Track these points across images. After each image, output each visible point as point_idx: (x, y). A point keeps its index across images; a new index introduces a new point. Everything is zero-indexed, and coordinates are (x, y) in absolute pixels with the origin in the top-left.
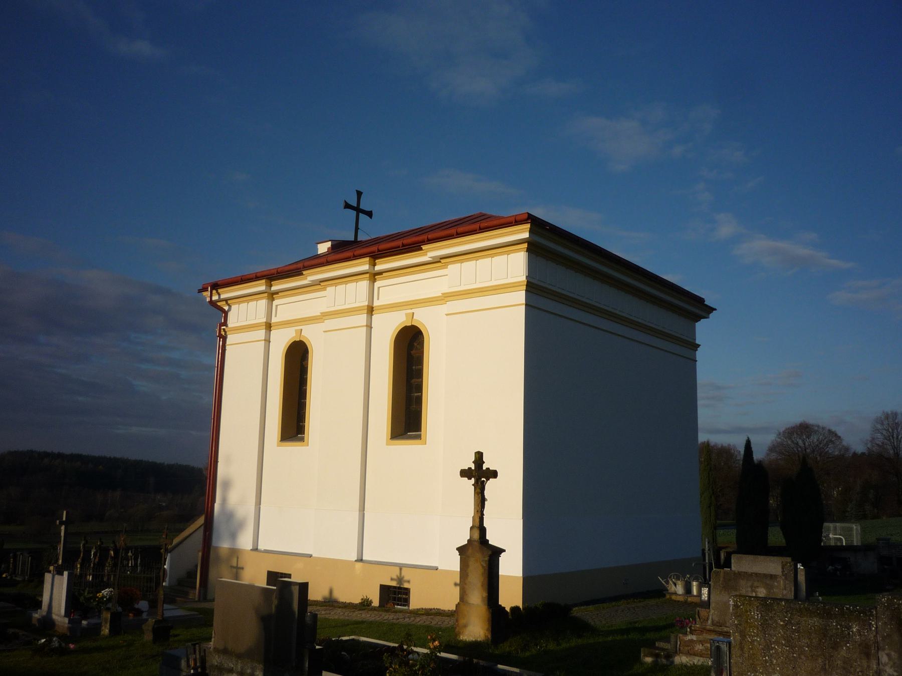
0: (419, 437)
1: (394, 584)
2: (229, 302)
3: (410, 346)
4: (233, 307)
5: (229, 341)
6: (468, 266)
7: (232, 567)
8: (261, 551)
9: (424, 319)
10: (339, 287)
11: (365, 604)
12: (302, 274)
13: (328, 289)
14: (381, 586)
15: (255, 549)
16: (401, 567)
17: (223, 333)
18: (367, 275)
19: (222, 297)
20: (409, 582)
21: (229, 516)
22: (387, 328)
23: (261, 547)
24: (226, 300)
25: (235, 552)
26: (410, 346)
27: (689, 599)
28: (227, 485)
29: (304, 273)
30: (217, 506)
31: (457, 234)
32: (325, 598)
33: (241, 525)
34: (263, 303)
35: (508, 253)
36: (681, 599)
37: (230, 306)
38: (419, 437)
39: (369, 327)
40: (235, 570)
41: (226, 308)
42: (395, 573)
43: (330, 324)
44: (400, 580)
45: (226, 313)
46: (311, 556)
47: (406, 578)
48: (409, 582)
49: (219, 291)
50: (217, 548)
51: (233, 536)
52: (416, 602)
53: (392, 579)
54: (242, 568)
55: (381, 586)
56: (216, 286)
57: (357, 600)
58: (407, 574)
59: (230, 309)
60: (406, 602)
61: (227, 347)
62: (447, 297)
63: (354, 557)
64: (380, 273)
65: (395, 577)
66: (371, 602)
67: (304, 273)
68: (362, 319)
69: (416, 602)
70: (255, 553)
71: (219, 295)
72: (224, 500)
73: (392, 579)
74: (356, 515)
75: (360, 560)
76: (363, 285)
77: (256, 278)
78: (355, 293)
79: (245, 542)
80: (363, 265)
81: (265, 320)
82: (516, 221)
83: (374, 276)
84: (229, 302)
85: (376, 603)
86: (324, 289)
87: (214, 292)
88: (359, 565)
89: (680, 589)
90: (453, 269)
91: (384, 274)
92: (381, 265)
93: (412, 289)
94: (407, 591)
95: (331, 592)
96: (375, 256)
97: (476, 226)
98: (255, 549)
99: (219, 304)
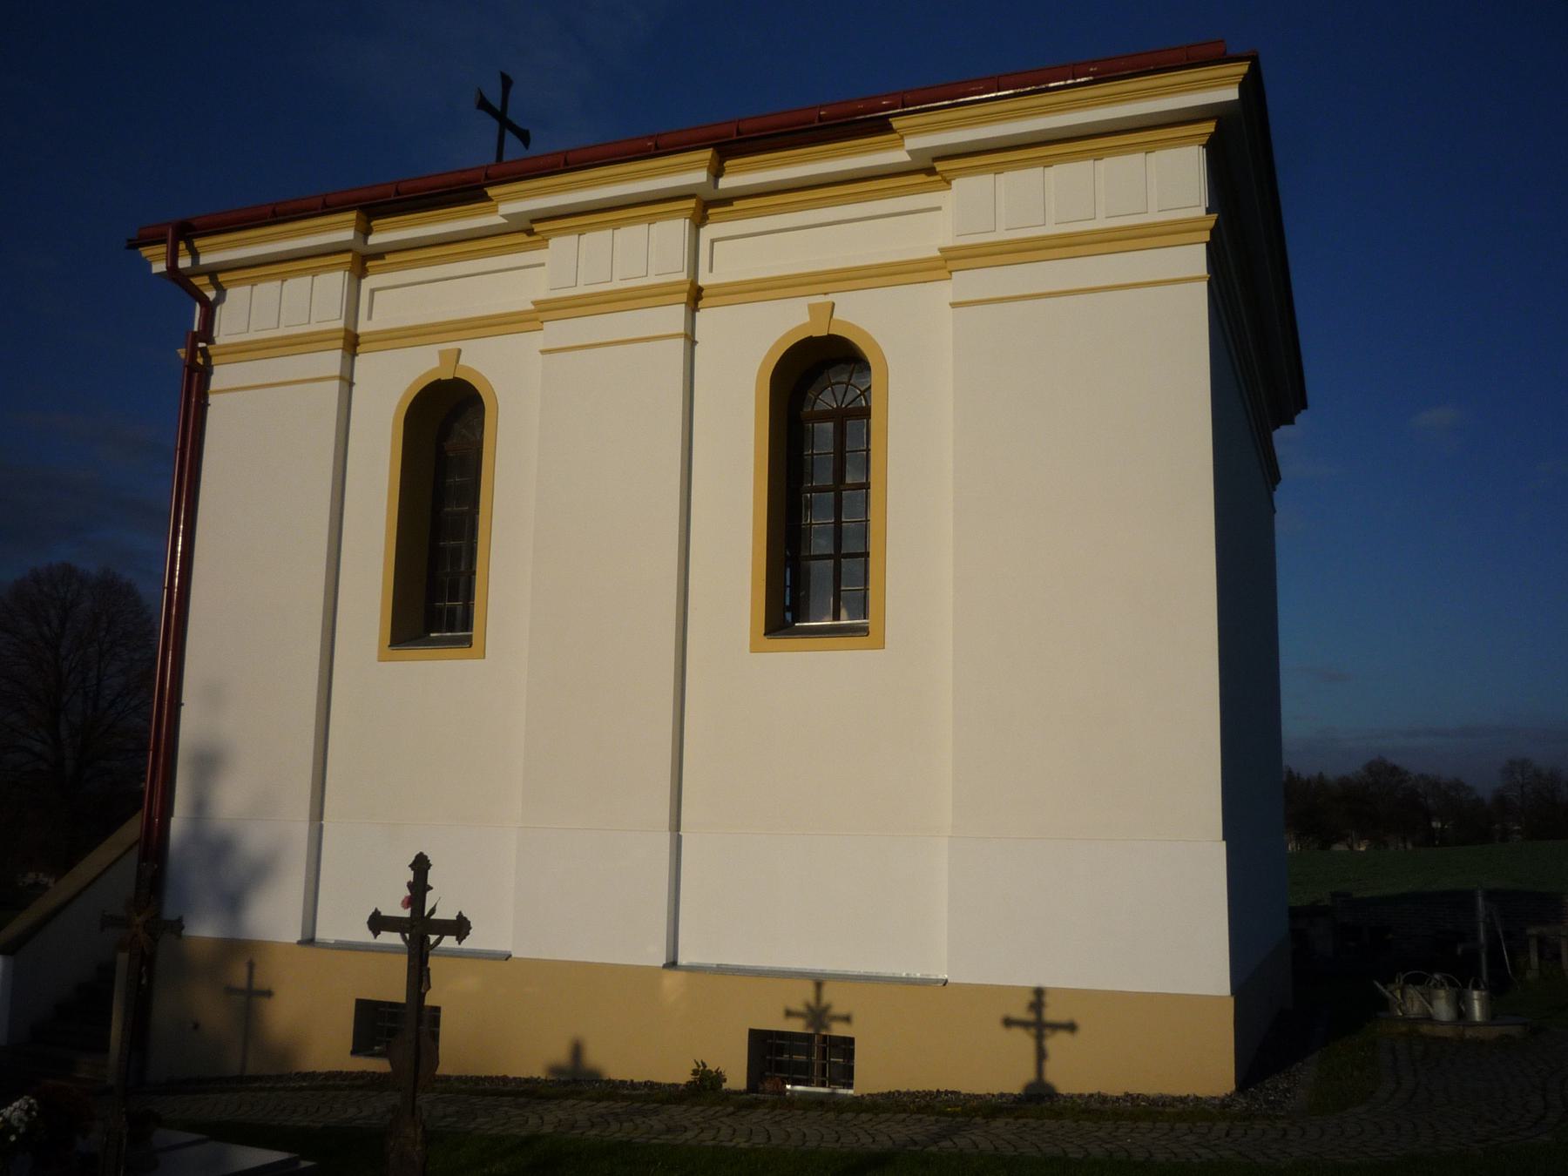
0: (467, 642)
1: (797, 1026)
2: (222, 278)
4: (233, 294)
5: (215, 382)
6: (596, 242)
7: (230, 990)
9: (482, 362)
10: (292, 283)
11: (706, 1084)
12: (485, 198)
13: (553, 242)
14: (754, 1034)
15: (309, 941)
16: (819, 982)
17: (200, 361)
18: (348, 257)
19: (205, 260)
20: (847, 1019)
21: (218, 849)
22: (387, 386)
23: (322, 934)
24: (213, 273)
25: (239, 949)
27: (1469, 1033)
28: (210, 763)
29: (491, 192)
30: (178, 824)
32: (555, 1070)
33: (261, 872)
35: (1149, 147)
36: (1448, 1032)
38: (467, 642)
39: (347, 381)
41: (211, 294)
42: (802, 996)
43: (557, 331)
44: (818, 1014)
45: (209, 310)
46: (508, 957)
47: (837, 1009)
48: (847, 1019)
49: (198, 243)
51: (233, 903)
52: (873, 1074)
53: (789, 1014)
54: (268, 994)
55: (754, 1034)
56: (186, 233)
57: (679, 1074)
58: (836, 999)
60: (847, 1078)
61: (212, 399)
62: (545, 311)
63: (662, 961)
64: (379, 254)
66: (718, 1078)
67: (896, 123)
69: (873, 1074)
70: (307, 950)
71: (195, 255)
72: (200, 806)
73: (789, 1014)
74: (665, 838)
75: (672, 964)
76: (673, 231)
77: (327, 207)
81: (340, 324)
82: (325, 205)
83: (362, 262)
84: (222, 278)
85: (736, 1077)
86: (543, 243)
87: (182, 246)
88: (671, 980)
89: (1442, 1008)
90: (561, 246)
92: (384, 235)
93: (448, 296)
94: (846, 1046)
95: (577, 1050)
98: (309, 941)
99: (197, 281)
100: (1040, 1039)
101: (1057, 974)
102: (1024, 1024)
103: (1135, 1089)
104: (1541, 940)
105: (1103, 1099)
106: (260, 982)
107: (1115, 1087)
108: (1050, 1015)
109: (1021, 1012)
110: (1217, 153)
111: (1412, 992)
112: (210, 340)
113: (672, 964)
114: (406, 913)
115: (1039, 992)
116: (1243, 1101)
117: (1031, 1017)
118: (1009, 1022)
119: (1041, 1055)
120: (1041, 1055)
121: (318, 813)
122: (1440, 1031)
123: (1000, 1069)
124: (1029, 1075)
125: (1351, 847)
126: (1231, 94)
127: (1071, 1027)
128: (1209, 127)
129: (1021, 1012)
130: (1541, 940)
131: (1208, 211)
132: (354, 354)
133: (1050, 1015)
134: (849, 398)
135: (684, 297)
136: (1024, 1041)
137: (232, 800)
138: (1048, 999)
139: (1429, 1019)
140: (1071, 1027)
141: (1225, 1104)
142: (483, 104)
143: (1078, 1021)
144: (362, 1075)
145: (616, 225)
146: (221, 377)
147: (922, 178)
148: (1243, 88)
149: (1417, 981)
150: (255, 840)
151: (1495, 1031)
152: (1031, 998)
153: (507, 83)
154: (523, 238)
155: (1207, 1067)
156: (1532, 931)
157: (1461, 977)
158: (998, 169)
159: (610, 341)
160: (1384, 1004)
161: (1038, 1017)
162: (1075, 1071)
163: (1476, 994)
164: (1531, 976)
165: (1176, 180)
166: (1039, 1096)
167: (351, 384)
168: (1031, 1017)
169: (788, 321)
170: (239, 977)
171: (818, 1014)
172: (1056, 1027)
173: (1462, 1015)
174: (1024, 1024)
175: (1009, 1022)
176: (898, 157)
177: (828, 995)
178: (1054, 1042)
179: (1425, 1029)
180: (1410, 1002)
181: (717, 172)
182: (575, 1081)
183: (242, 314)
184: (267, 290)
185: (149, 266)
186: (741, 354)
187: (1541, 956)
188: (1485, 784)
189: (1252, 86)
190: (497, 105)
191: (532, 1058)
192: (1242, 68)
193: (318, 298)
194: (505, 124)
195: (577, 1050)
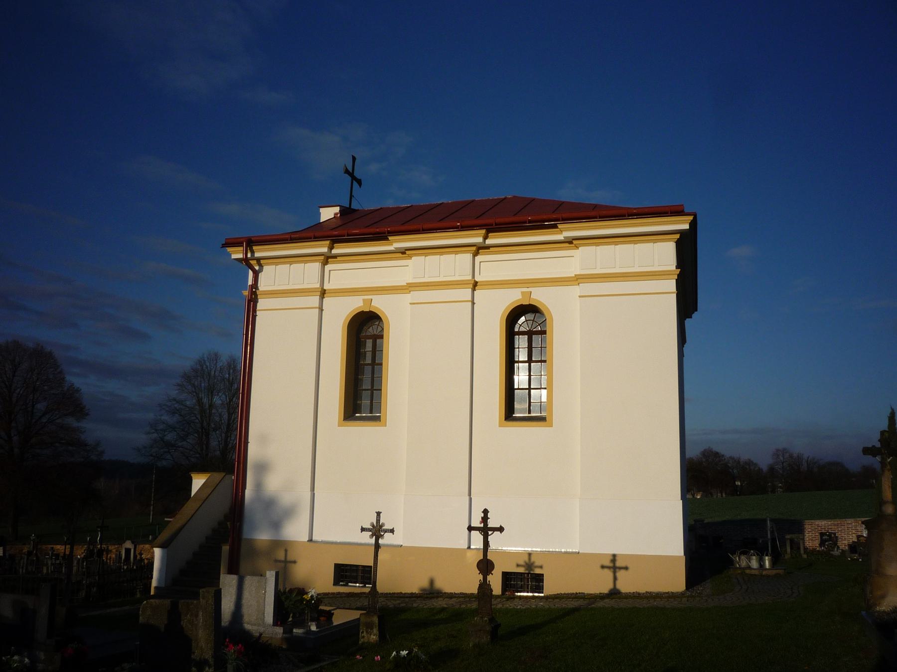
1: (521, 570)
2: (262, 262)
3: (365, 332)
4: (265, 268)
5: (260, 306)
6: (433, 260)
7: (276, 561)
8: (316, 542)
9: (380, 304)
14: (503, 573)
19: (257, 255)
20: (541, 567)
21: (269, 504)
23: (314, 538)
24: (258, 260)
25: (279, 544)
26: (365, 332)
27: (764, 573)
28: (263, 468)
29: (390, 238)
30: (249, 493)
31: (315, 237)
32: (423, 590)
33: (289, 513)
34: (316, 266)
36: (757, 572)
37: (261, 266)
39: (321, 310)
40: (283, 564)
41: (257, 268)
44: (529, 565)
45: (256, 274)
47: (537, 564)
48: (541, 567)
49: (254, 248)
50: (251, 542)
51: (277, 525)
52: (551, 587)
53: (518, 565)
54: (295, 562)
55: (503, 573)
56: (250, 243)
59: (261, 270)
60: (540, 589)
61: (258, 313)
62: (410, 287)
64: (335, 257)
65: (522, 563)
67: (390, 238)
68: (315, 300)
69: (551, 587)
70: (311, 544)
71: (253, 252)
72: (259, 486)
73: (518, 565)
74: (468, 498)
76: (315, 267)
78: (456, 266)
79: (295, 531)
80: (322, 248)
83: (327, 259)
84: (262, 262)
89: (754, 564)
90: (417, 261)
91: (492, 249)
95: (432, 582)
96: (491, 229)
97: (312, 234)
98: (311, 540)
99: (252, 262)
100: (615, 573)
101: (621, 549)
102: (609, 568)
103: (649, 590)
104: (792, 541)
105: (639, 594)
106: (289, 558)
107: (642, 590)
108: (618, 564)
109: (607, 563)
110: (679, 245)
111: (743, 557)
112: (257, 288)
113: (469, 548)
114: (482, 525)
115: (614, 556)
116: (688, 593)
117: (611, 565)
118: (603, 567)
119: (615, 579)
120: (615, 579)
121: (313, 489)
122: (753, 572)
123: (601, 584)
124: (611, 586)
125: (693, 496)
126: (686, 226)
127: (626, 568)
128: (678, 236)
129: (607, 563)
130: (792, 541)
131: (677, 267)
132: (323, 298)
133: (618, 564)
134: (534, 326)
135: (471, 286)
136: (609, 574)
137: (274, 483)
138: (617, 558)
139: (749, 568)
140: (626, 568)
141: (682, 594)
142: (347, 171)
143: (629, 566)
144: (339, 593)
145: (442, 254)
146: (262, 304)
147: (567, 245)
148: (690, 224)
149: (744, 553)
150: (286, 499)
151: (774, 572)
152: (612, 558)
153: (354, 159)
154: (400, 255)
155: (675, 581)
156: (788, 537)
157: (761, 553)
158: (597, 245)
159: (436, 298)
160: (731, 562)
161: (614, 565)
162: (627, 584)
163: (767, 558)
164: (787, 557)
165: (665, 255)
166: (614, 593)
167: (322, 310)
168: (611, 565)
169: (513, 297)
170: (281, 556)
171: (529, 565)
172: (620, 568)
173: (762, 566)
174: (609, 568)
175: (603, 567)
176: (560, 237)
177: (533, 559)
178: (620, 574)
179: (747, 571)
180: (742, 561)
181: (486, 238)
182: (431, 593)
183: (271, 278)
184: (283, 268)
185: (230, 255)
186: (494, 308)
187: (791, 549)
188: (764, 461)
189: (693, 224)
190: (351, 171)
191: (413, 584)
192: (691, 218)
193: (306, 274)
194: (354, 178)
195: (432, 582)
